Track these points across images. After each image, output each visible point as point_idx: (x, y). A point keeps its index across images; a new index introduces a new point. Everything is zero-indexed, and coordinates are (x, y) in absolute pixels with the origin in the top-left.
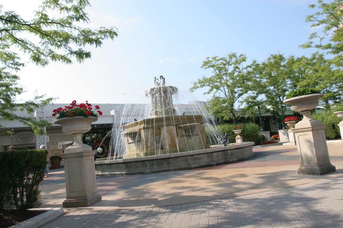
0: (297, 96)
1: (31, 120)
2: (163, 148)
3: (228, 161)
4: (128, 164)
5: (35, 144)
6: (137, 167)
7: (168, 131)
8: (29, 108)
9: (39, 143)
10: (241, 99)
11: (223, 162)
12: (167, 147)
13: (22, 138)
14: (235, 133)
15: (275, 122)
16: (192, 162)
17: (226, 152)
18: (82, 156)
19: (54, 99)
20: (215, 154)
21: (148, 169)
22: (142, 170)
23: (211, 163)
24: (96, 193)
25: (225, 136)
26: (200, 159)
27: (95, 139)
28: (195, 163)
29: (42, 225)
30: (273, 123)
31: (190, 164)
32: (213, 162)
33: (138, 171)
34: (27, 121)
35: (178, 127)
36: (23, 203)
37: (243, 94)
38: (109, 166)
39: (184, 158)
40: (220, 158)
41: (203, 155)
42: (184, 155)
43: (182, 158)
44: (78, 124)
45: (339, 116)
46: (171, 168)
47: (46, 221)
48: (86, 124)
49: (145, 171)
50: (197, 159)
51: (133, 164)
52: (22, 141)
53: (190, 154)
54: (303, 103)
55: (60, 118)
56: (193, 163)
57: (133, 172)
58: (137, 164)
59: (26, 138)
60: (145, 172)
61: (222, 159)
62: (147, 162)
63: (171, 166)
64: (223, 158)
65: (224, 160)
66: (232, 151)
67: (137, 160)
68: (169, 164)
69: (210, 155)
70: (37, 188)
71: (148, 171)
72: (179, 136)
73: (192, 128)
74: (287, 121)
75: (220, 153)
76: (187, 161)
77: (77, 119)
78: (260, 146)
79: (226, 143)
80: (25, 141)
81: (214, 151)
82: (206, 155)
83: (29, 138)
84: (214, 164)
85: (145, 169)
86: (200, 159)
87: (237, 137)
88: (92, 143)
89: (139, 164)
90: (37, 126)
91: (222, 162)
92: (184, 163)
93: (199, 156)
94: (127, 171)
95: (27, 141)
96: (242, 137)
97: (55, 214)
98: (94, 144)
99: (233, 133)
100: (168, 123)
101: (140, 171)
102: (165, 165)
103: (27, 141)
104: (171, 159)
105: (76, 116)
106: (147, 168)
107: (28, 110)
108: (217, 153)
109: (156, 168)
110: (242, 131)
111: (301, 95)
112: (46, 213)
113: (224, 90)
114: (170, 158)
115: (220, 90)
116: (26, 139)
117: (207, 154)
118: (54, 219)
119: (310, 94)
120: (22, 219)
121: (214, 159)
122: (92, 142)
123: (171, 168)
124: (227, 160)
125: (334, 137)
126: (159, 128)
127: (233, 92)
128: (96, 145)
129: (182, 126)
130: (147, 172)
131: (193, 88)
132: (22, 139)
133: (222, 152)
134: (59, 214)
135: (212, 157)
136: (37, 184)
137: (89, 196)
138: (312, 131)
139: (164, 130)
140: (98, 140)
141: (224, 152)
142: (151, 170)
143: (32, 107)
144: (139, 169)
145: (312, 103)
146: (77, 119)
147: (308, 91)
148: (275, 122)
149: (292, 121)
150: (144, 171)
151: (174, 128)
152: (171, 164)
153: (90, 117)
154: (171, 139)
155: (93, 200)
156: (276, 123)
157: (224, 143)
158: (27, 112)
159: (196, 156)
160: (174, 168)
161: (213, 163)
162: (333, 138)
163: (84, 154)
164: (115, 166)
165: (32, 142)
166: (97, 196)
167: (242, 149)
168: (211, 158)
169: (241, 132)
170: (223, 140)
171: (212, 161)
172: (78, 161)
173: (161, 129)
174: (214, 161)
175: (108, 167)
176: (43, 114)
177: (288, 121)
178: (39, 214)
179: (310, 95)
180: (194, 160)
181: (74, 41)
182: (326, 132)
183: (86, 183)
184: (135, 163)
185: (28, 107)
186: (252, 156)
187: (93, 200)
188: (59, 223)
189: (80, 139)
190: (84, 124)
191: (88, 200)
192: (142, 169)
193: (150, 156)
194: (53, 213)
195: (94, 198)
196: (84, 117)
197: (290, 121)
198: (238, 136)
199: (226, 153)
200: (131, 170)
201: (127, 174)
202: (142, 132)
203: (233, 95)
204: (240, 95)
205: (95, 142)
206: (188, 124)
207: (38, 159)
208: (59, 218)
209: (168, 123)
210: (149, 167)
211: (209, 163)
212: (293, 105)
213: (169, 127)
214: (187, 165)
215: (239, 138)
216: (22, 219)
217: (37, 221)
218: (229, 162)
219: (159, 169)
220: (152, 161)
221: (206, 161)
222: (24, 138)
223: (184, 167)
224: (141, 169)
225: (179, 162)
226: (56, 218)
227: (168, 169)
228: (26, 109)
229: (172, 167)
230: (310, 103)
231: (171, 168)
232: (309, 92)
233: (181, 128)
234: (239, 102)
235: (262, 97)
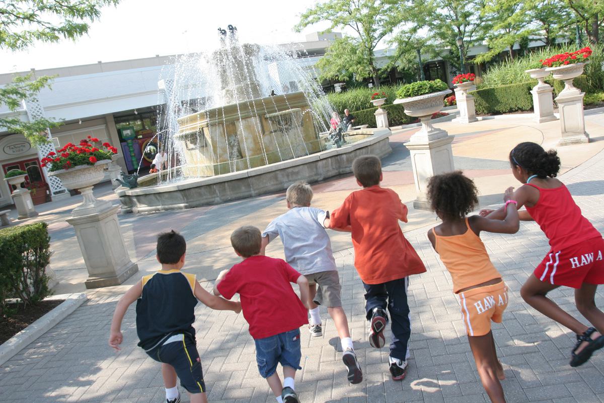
0: (409, 96)
1: (18, 122)
2: (243, 156)
3: (343, 171)
4: (186, 191)
5: (36, 154)
6: (200, 195)
7: (249, 128)
8: (10, 101)
9: (43, 151)
10: (387, 37)
11: (334, 174)
12: (248, 155)
13: (13, 147)
14: (374, 104)
15: (454, 69)
16: (285, 179)
17: (338, 157)
18: (98, 220)
19: (50, 78)
20: (320, 163)
21: (218, 197)
22: (209, 198)
23: (316, 178)
24: (127, 264)
25: (338, 131)
26: (297, 173)
27: (140, 132)
28: (290, 181)
29: (61, 321)
30: (451, 72)
31: (281, 183)
32: (319, 177)
33: (202, 202)
34: (13, 124)
35: (262, 118)
36: (30, 295)
37: (386, 34)
38: (157, 196)
39: (272, 174)
40: (330, 168)
41: (301, 167)
42: (270, 171)
43: (269, 176)
44: (83, 176)
45: (533, 76)
46: (253, 192)
47: (64, 316)
48: (94, 174)
49: (213, 200)
50: (293, 173)
51: (193, 191)
52: (14, 152)
53: (280, 169)
54: (418, 108)
55: (53, 171)
56: (287, 181)
57: (194, 204)
58: (200, 191)
59: (18, 146)
60: (213, 201)
61: (333, 169)
62: (214, 187)
63: (252, 189)
64: (334, 167)
65: (337, 171)
66: (348, 155)
67: (198, 185)
68: (249, 186)
69: (314, 165)
70: (44, 274)
71: (218, 199)
72: (266, 133)
73: (287, 119)
74: (456, 82)
75: (330, 159)
76: (276, 178)
77: (80, 170)
78: (415, 124)
79: (340, 142)
80: (19, 151)
81: (319, 159)
82: (306, 166)
83: (24, 146)
84: (319, 179)
85: (212, 198)
86: (297, 173)
87: (377, 112)
88: (137, 140)
89: (203, 190)
90: (33, 131)
91: (333, 175)
92: (272, 183)
93: (296, 170)
94: (187, 203)
95: (22, 150)
96: (387, 110)
97: (75, 304)
98: (140, 141)
99: (372, 105)
100: (247, 114)
101: (206, 201)
102: (243, 188)
103: (22, 150)
104: (250, 179)
105: (77, 165)
106: (215, 196)
107: (9, 103)
108: (324, 161)
109: (229, 194)
110: (386, 101)
111: (416, 96)
112: (62, 304)
113: (356, 25)
114: (249, 177)
115: (349, 25)
116: (19, 147)
117: (308, 165)
118: (75, 311)
119: (427, 93)
120: (32, 318)
121: (321, 171)
122: (136, 137)
123: (253, 192)
124: (341, 170)
125: (529, 108)
126: (232, 124)
127: (369, 31)
128: (143, 142)
129: (268, 116)
130: (216, 201)
131: (300, 25)
132: (12, 148)
133: (333, 158)
134: (81, 303)
135: (316, 168)
136: (43, 269)
137: (119, 270)
138: (430, 148)
139: (241, 125)
140: (145, 133)
141: (336, 158)
142: (223, 198)
143: (14, 96)
144: (205, 197)
145: (431, 106)
146: (80, 170)
147: (426, 89)
148: (454, 69)
149: (466, 81)
150: (211, 200)
151: (255, 121)
152: (251, 186)
153: (98, 162)
154: (254, 140)
155: (125, 275)
156: (455, 73)
157: (336, 142)
158: (8, 107)
159: (290, 170)
160: (256, 192)
161: (318, 178)
162: (528, 109)
163: (100, 217)
164: (166, 195)
165: (32, 152)
166: (130, 267)
167: (367, 148)
168: (315, 170)
169: (384, 103)
170: (334, 137)
171: (317, 174)
172: (94, 227)
173: (236, 123)
174: (321, 174)
175: (157, 198)
176: (38, 103)
177: (458, 83)
178: (54, 308)
179: (426, 96)
180: (288, 176)
181: (53, 12)
182: (518, 99)
183: (111, 255)
184: (196, 190)
185: (9, 98)
186: (387, 156)
187: (125, 275)
188: (81, 318)
189: (92, 194)
190: (91, 173)
191: (118, 277)
192: (209, 197)
193: (221, 173)
194: (72, 303)
195: (127, 272)
196: (88, 166)
197: (461, 83)
198: (380, 111)
199: (339, 159)
200: (192, 200)
201: (186, 207)
202: (207, 132)
203: (368, 34)
204: (383, 35)
205: (141, 137)
206: (278, 113)
207: (35, 240)
208: (81, 308)
209: (247, 114)
210: (219, 194)
211: (312, 178)
212: (408, 108)
213: (249, 119)
214: (277, 184)
215: (381, 114)
216: (32, 318)
217: (52, 319)
218: (345, 172)
219: (234, 196)
220: (223, 184)
221: (307, 175)
222: (16, 146)
223: (272, 188)
224: (207, 197)
225: (264, 181)
226: (78, 308)
227: (247, 194)
228: (5, 102)
229: (254, 190)
230: (428, 107)
231: (253, 192)
232: (427, 91)
233: (266, 119)
234: (384, 42)
235: (424, 33)
